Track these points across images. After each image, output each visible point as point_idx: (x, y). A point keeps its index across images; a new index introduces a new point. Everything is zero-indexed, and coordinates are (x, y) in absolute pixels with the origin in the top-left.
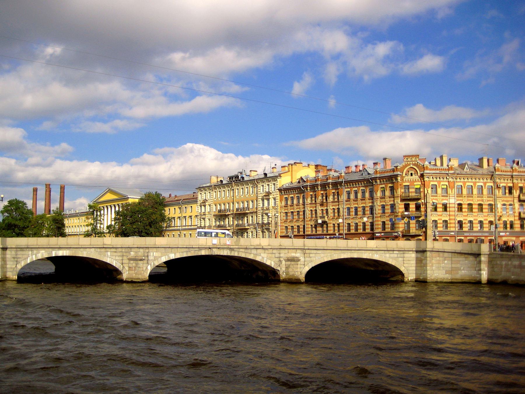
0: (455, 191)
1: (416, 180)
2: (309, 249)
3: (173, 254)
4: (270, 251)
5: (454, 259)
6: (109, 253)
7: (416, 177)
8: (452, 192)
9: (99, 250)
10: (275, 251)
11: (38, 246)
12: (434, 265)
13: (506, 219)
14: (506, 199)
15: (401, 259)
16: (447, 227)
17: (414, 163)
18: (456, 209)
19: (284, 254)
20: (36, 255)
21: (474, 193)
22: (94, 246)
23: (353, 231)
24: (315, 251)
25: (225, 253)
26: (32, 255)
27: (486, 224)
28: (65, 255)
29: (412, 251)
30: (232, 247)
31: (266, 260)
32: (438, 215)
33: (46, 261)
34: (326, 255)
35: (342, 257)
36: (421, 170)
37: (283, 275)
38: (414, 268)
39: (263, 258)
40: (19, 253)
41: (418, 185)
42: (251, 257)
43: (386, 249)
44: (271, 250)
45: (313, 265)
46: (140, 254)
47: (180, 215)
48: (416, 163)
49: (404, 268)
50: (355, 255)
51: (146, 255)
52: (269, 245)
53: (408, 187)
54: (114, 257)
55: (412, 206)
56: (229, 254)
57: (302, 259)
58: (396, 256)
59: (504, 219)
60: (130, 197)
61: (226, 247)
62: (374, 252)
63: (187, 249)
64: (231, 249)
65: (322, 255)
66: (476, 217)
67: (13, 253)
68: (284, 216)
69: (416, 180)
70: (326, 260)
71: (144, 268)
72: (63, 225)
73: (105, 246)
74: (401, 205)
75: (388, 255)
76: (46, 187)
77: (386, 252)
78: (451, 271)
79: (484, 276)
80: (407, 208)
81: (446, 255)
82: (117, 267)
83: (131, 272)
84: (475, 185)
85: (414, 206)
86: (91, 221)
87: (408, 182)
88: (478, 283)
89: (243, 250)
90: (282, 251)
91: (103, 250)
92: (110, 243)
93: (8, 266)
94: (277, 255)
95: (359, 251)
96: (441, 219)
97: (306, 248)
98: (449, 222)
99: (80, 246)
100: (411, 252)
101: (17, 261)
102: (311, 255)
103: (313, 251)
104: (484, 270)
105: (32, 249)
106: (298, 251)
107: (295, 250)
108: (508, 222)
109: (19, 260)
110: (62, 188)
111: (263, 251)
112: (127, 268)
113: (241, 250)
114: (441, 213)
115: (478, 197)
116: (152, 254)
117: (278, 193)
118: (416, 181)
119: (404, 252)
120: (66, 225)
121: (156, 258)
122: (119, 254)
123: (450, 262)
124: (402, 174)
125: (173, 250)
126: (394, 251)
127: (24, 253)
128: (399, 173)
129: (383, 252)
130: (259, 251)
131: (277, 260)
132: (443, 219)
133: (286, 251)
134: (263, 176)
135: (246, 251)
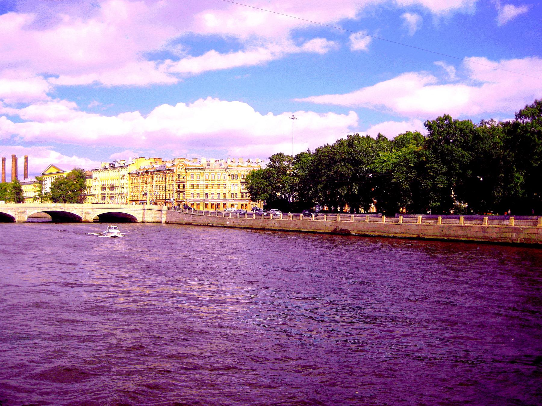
4: (78, 209)
7: (183, 170)
16: (207, 197)
18: (205, 187)
19: (84, 211)
23: (158, 199)
37: (83, 220)
41: (184, 174)
55: (181, 185)
57: (92, 213)
59: (232, 192)
64: (61, 208)
66: (216, 191)
72: (21, 191)
76: (12, 158)
79: (164, 220)
80: (179, 186)
86: (38, 189)
88: (161, 223)
108: (234, 194)
110: (26, 159)
112: (17, 216)
120: (24, 191)
121: (30, 212)
128: (175, 168)
134: (123, 165)
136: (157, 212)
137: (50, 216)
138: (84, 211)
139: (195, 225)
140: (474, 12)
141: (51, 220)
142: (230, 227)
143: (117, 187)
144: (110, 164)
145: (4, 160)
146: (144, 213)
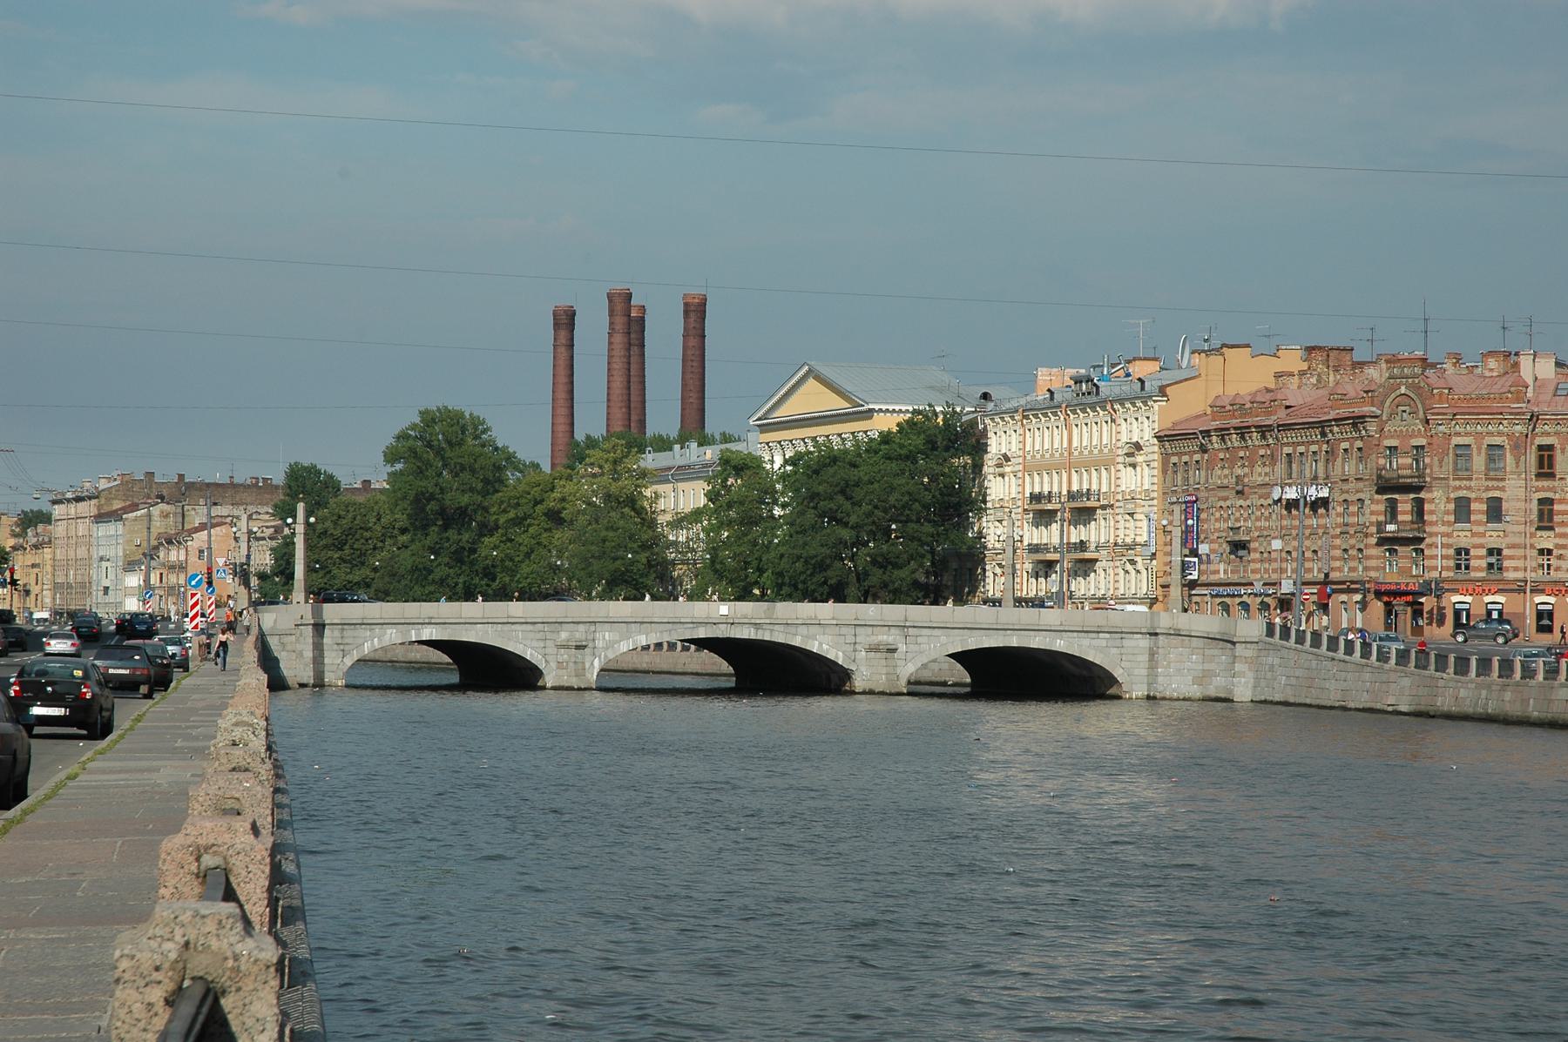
0: (1532, 458)
2: (914, 627)
5: (1207, 652)
10: (844, 630)
12: (1172, 665)
15: (1115, 651)
19: (865, 637)
22: (490, 621)
32: (1474, 535)
38: (1144, 672)
40: (349, 633)
42: (797, 641)
44: (838, 628)
46: (578, 635)
49: (1121, 670)
51: (590, 637)
52: (833, 619)
53: (501, 542)
57: (902, 648)
60: (877, 407)
61: (746, 621)
67: (337, 633)
74: (1378, 502)
78: (1201, 679)
85: (1408, 507)
89: (781, 628)
90: (859, 630)
93: (326, 661)
94: (850, 639)
98: (1505, 552)
103: (925, 631)
104: (1242, 674)
105: (374, 627)
106: (893, 630)
110: (696, 312)
112: (553, 665)
114: (1481, 529)
117: (1156, 449)
119: (1123, 635)
121: (610, 645)
124: (1379, 412)
129: (1075, 634)
130: (813, 629)
136: (1215, 651)
137: (725, 667)
138: (865, 637)
139: (891, 694)
140: (380, 482)
141: (731, 682)
142: (1449, 717)
143: (1104, 507)
144: (1078, 381)
145: (565, 321)
146: (1152, 654)
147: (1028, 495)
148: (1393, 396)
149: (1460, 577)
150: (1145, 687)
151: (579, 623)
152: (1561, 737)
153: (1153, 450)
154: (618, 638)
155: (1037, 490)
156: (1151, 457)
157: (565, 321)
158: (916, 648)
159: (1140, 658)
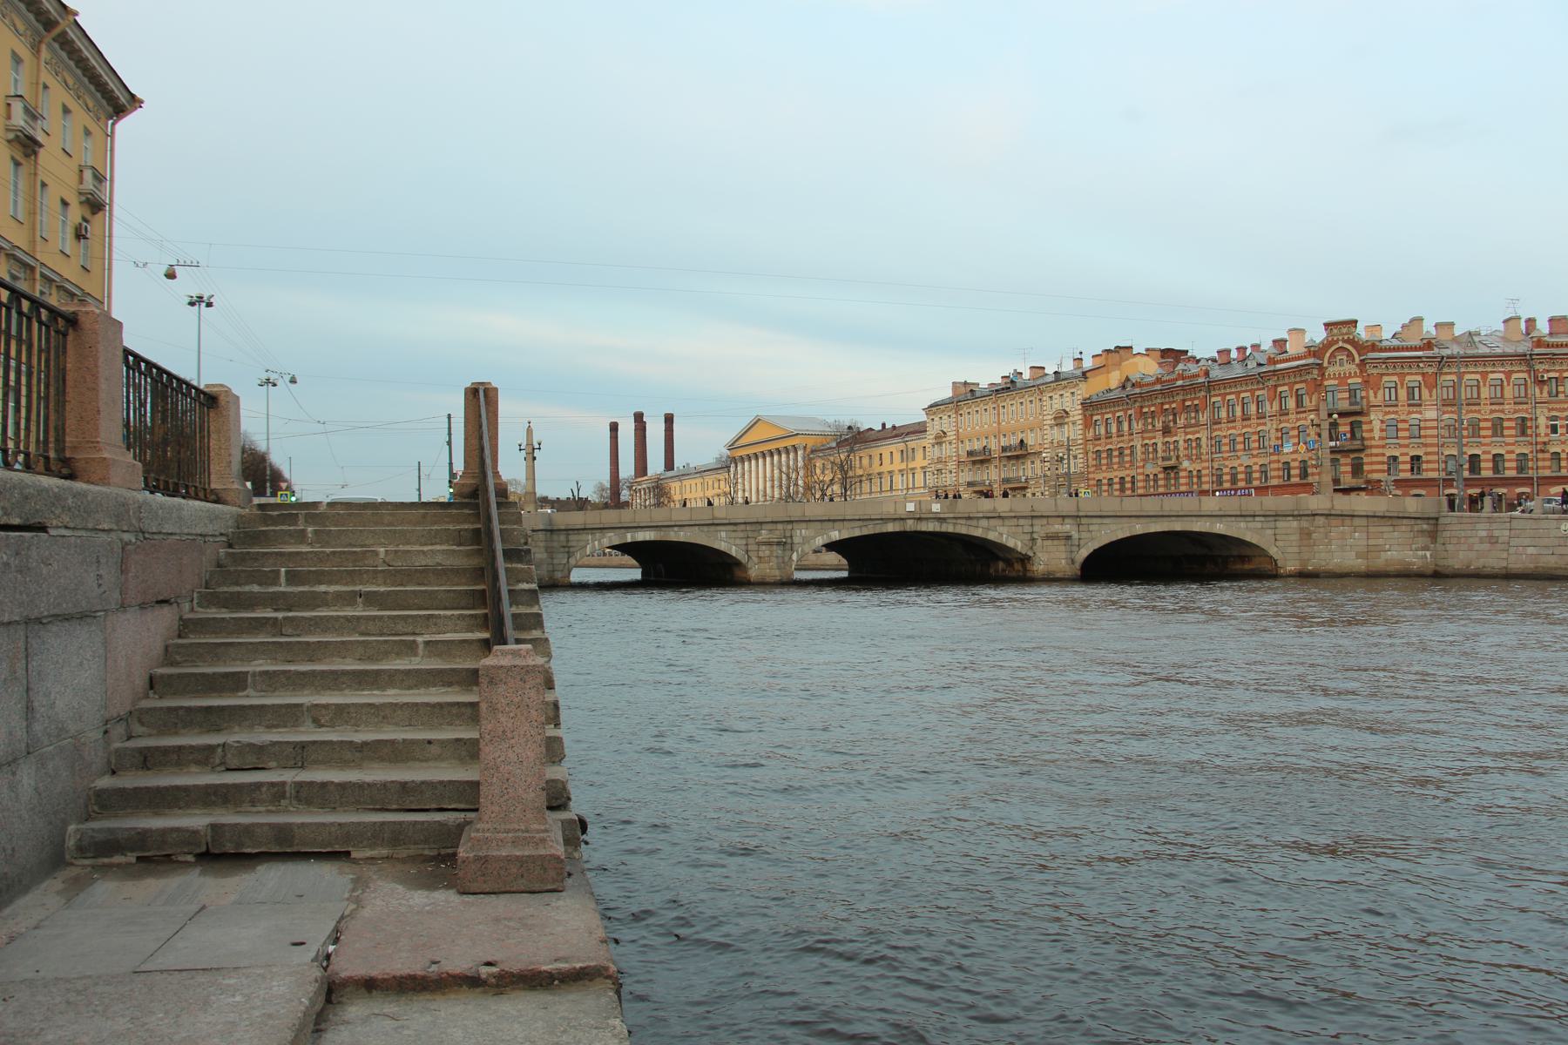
1: (1350, 373)
2: (1086, 516)
3: (837, 533)
5: (1372, 529)
6: (723, 534)
7: (1353, 368)
8: (1431, 396)
9: (705, 529)
10: (1022, 522)
11: (602, 526)
12: (1334, 542)
13: (1558, 450)
14: (1558, 406)
15: (1269, 532)
17: (1346, 337)
20: (599, 541)
21: (1483, 396)
24: (1099, 521)
25: (930, 527)
26: (593, 541)
27: (1487, 461)
28: (648, 539)
29: (1293, 516)
30: (942, 516)
31: (1007, 539)
32: (1401, 446)
33: (615, 600)
34: (1120, 526)
35: (1152, 530)
36: (1362, 352)
39: (1001, 534)
42: (978, 533)
43: (1239, 513)
45: (1096, 545)
47: (903, 466)
48: (1351, 337)
49: (1276, 549)
50: (1178, 526)
51: (788, 534)
54: (732, 541)
56: (938, 529)
57: (1075, 535)
58: (1259, 525)
61: (931, 516)
62: (1214, 519)
63: (860, 523)
64: (942, 520)
65: (1113, 527)
68: (1093, 459)
69: (1350, 373)
70: (1121, 535)
71: (786, 559)
73: (716, 522)
75: (1243, 525)
77: (1240, 519)
81: (1357, 521)
82: (738, 557)
83: (762, 566)
84: (1508, 378)
87: (1335, 378)
90: (1036, 521)
91: (712, 528)
92: (723, 515)
95: (1185, 519)
96: (1407, 454)
97: (1081, 514)
98: (1424, 458)
99: (673, 523)
100: (1291, 518)
101: (568, 552)
102: (1091, 528)
103: (1095, 521)
107: (1060, 519)
109: (571, 550)
110: (669, 419)
111: (999, 522)
113: (959, 521)
115: (1491, 404)
116: (798, 532)
117: (1080, 412)
118: (1350, 377)
121: (806, 540)
122: (742, 535)
123: (1365, 535)
125: (837, 524)
126: (1254, 516)
127: (580, 537)
129: (1233, 519)
130: (993, 522)
131: (1028, 537)
132: (1411, 454)
133: (1044, 521)
135: (969, 522)
138: (1040, 528)
145: (614, 428)
147: (963, 453)
148: (1333, 348)
149: (1414, 477)
150: (1297, 563)
151: (776, 522)
152: (1560, 603)
153: (1076, 414)
154: (812, 534)
155: (968, 449)
156: (1076, 418)
157: (614, 428)
158: (1088, 535)
159: (1293, 537)
